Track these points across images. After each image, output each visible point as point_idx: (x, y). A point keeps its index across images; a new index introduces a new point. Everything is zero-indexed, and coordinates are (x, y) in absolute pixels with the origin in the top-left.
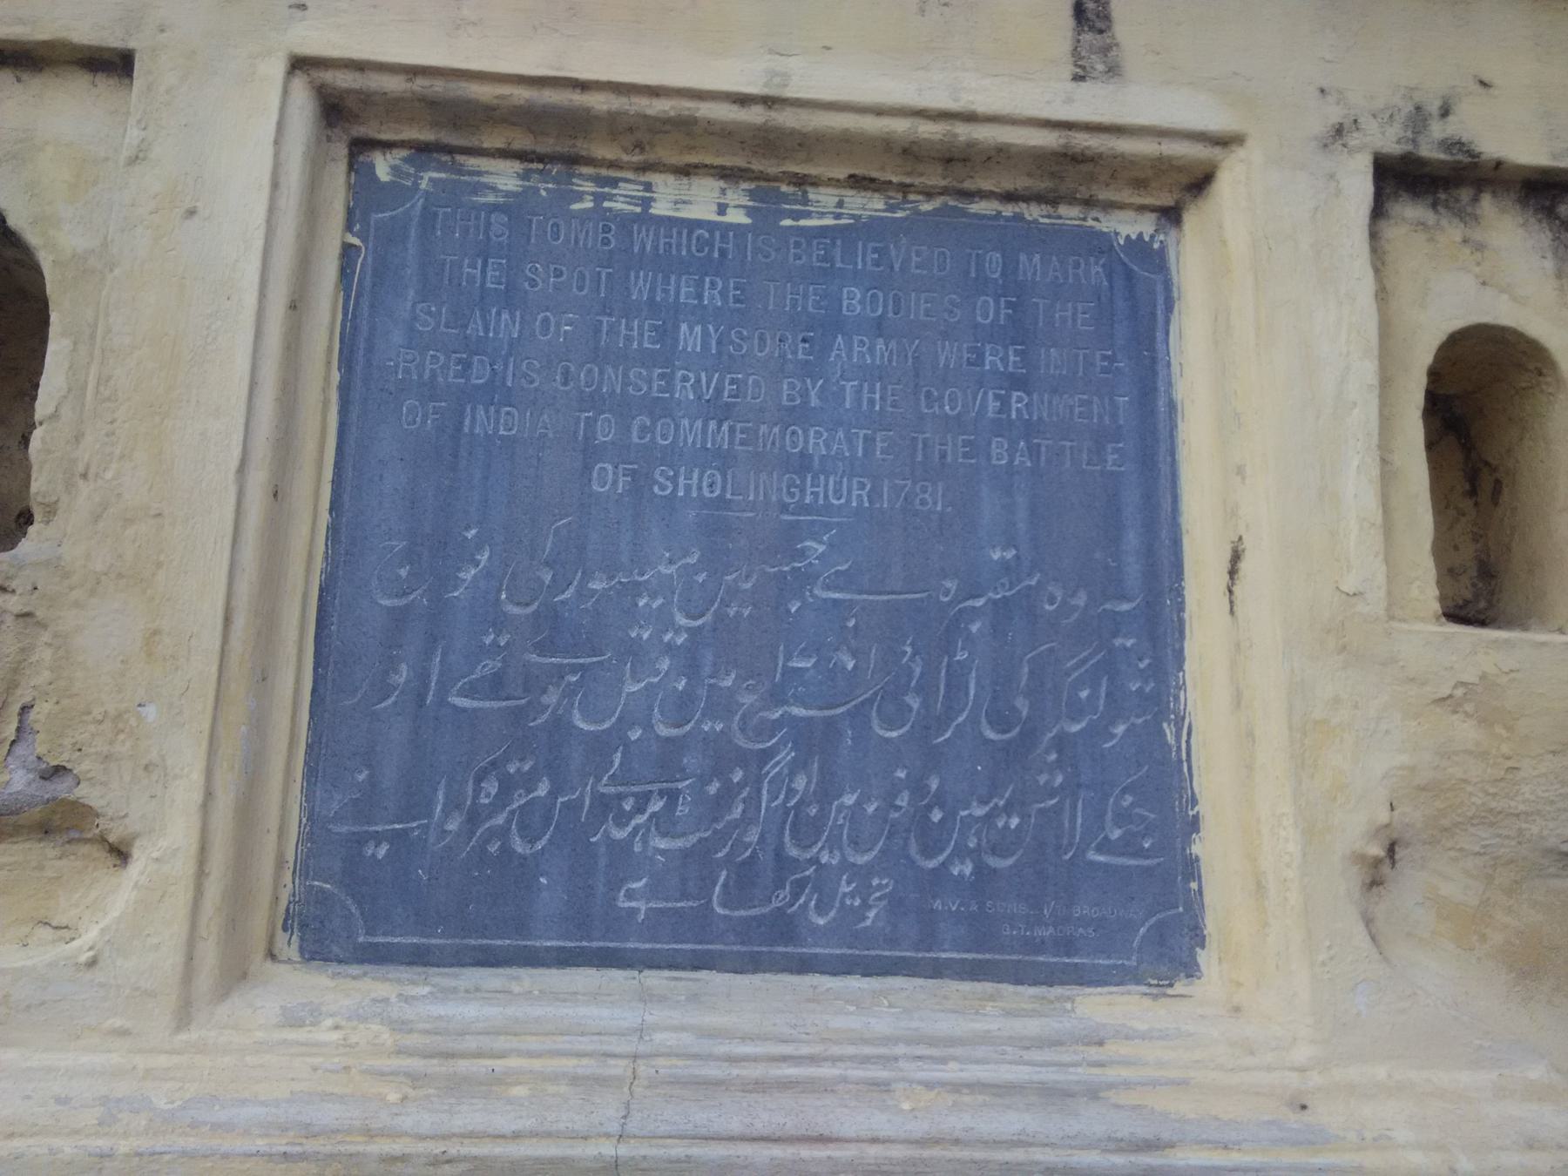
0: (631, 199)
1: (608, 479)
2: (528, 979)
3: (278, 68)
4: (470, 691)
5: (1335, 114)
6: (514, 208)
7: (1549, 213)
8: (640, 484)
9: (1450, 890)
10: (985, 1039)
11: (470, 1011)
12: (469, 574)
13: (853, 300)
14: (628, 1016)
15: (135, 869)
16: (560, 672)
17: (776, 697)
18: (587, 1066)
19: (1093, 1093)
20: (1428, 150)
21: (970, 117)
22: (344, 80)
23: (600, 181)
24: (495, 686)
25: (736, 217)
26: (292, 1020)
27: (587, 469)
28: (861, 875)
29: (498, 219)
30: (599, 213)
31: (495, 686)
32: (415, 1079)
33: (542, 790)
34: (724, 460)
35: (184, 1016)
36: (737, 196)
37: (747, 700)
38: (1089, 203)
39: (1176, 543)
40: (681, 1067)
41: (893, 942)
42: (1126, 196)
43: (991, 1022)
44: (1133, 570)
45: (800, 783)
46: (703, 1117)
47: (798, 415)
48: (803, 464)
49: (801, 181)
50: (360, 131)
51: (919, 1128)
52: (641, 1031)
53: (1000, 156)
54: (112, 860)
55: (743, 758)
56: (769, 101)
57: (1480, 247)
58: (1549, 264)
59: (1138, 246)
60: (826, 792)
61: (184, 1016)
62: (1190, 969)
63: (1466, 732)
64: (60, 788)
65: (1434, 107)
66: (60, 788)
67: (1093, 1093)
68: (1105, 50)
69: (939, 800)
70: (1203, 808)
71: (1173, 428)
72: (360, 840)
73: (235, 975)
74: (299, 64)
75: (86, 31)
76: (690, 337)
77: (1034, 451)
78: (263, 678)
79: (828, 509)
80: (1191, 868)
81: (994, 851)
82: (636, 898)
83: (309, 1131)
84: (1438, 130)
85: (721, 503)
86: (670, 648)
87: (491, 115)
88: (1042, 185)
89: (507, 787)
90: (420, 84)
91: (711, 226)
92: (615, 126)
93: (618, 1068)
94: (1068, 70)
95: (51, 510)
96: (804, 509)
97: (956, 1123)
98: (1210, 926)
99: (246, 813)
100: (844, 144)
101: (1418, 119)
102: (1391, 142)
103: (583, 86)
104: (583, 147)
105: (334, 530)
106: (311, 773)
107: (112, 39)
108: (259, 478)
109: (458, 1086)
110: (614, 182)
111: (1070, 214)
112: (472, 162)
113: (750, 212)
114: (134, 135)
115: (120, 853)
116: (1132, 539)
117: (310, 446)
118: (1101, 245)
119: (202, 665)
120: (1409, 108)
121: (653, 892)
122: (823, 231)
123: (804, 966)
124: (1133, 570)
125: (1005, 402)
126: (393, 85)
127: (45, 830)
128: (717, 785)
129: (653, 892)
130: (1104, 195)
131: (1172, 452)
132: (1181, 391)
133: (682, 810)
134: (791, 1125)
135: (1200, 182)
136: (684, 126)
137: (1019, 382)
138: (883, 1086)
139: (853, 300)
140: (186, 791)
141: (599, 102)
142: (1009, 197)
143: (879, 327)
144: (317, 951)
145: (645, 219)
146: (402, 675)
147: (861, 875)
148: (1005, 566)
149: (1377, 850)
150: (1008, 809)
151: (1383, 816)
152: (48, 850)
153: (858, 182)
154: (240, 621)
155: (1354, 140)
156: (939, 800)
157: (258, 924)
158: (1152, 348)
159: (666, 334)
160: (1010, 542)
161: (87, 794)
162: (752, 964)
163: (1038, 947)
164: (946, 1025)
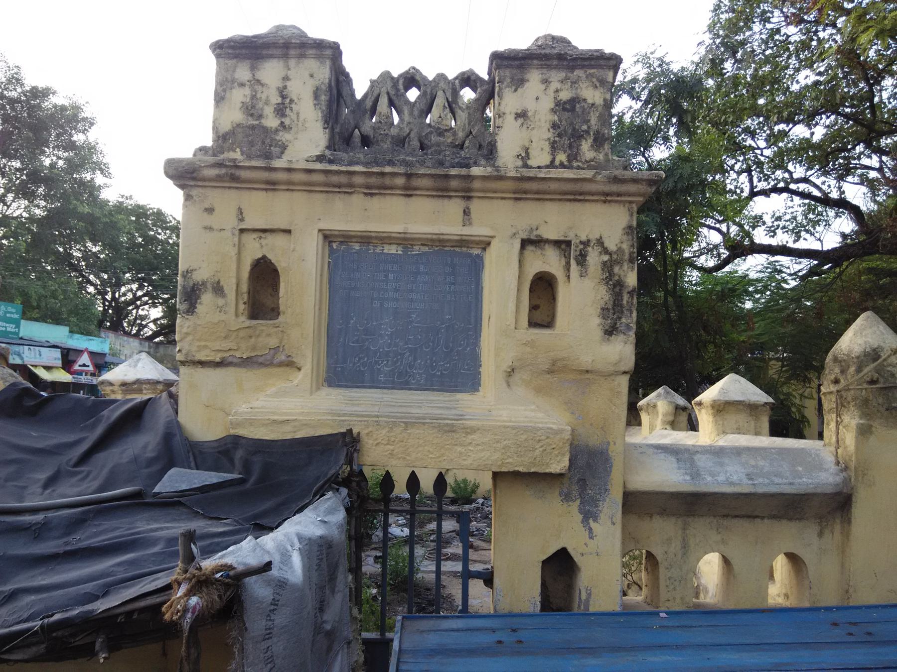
0: (380, 250)
1: (376, 304)
2: (364, 390)
3: (316, 232)
4: (353, 343)
5: (514, 231)
6: (358, 252)
7: (559, 247)
8: (382, 305)
9: (524, 377)
10: (438, 400)
11: (355, 394)
12: (352, 322)
13: (422, 268)
14: (381, 396)
15: (302, 371)
16: (368, 339)
17: (406, 343)
18: (373, 403)
19: (455, 408)
20: (533, 237)
21: (443, 234)
22: (328, 233)
23: (373, 246)
24: (357, 341)
25: (400, 252)
26: (327, 395)
27: (372, 302)
28: (420, 374)
29: (356, 255)
30: (374, 253)
31: (357, 341)
32: (347, 403)
33: (366, 359)
34: (397, 300)
35: (311, 394)
36: (400, 248)
37: (401, 344)
38: (468, 247)
39: (481, 314)
40: (388, 403)
41: (425, 385)
42: (475, 246)
43: (441, 398)
44: (473, 320)
45: (410, 358)
46: (390, 410)
47: (412, 291)
48: (412, 300)
49: (412, 245)
50: (331, 239)
51: (425, 412)
52: (382, 398)
53: (448, 241)
54: (297, 370)
55: (400, 354)
56: (405, 233)
57: (544, 255)
58: (558, 258)
59: (478, 256)
60: (415, 359)
61: (311, 394)
62: (478, 390)
63: (528, 349)
64: (290, 359)
65: (535, 228)
66: (290, 359)
67: (455, 408)
68: (469, 220)
69: (435, 362)
70: (482, 363)
71: (482, 291)
72: (336, 367)
73: (318, 389)
74: (320, 230)
75: (283, 226)
76: (391, 276)
77: (455, 297)
78: (320, 340)
79: (416, 309)
80: (479, 373)
81: (445, 370)
82: (382, 378)
83: (332, 410)
84: (535, 233)
85: (396, 308)
86: (387, 335)
87: (354, 237)
88: (459, 244)
89: (360, 359)
90: (341, 233)
91: (395, 254)
92: (376, 238)
93: (378, 403)
94: (461, 224)
95: (284, 313)
96: (411, 309)
97: (430, 412)
98: (482, 383)
99: (318, 364)
100: (419, 239)
101: (532, 230)
102: (525, 237)
103: (370, 232)
104: (371, 241)
105: (329, 314)
106: (327, 357)
107: (288, 228)
108: (317, 307)
109: (353, 405)
110: (377, 246)
111: (464, 249)
112: (351, 244)
113: (402, 251)
114: (292, 246)
115: (299, 369)
116: (473, 314)
117: (324, 300)
118: (470, 255)
119: (311, 339)
120: (529, 228)
121: (384, 377)
122: (416, 254)
123: (410, 389)
124: (473, 320)
125: (450, 287)
126: (336, 233)
127: (287, 365)
128: (771, 372)
129: (384, 377)
130: (471, 246)
131: (482, 297)
132: (484, 285)
133: (389, 363)
134: (405, 411)
135: (489, 244)
136: (390, 238)
137: (453, 284)
138: (421, 407)
139: (422, 268)
140: (309, 360)
141: (373, 234)
142: (452, 247)
143: (427, 273)
144: (330, 385)
145: (383, 253)
146: (341, 340)
147: (420, 374)
148: (449, 319)
149: (509, 370)
150: (447, 364)
151: (511, 364)
152: (288, 369)
153: (422, 245)
154: (316, 332)
155: (517, 236)
156: (435, 362)
157: (321, 381)
158: (479, 276)
159: (386, 276)
160: (450, 315)
161: (294, 360)
162: (402, 389)
163: (451, 386)
164: (432, 398)
